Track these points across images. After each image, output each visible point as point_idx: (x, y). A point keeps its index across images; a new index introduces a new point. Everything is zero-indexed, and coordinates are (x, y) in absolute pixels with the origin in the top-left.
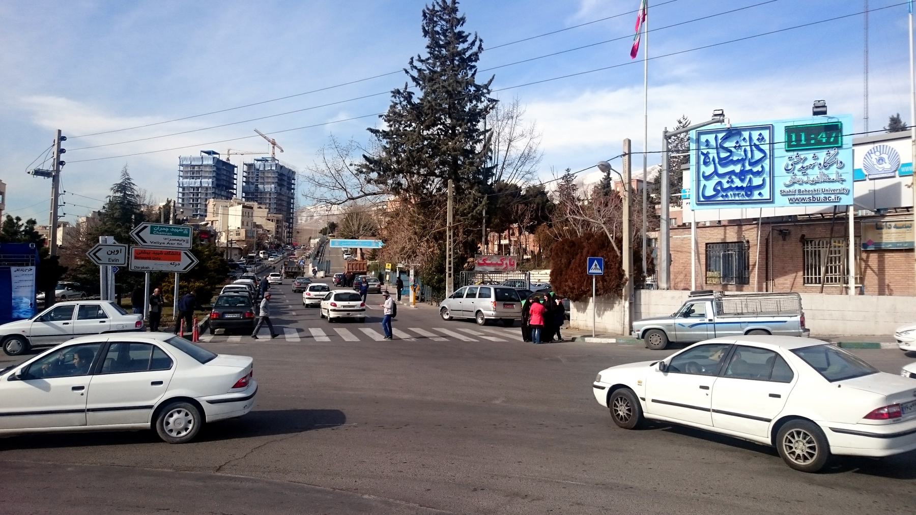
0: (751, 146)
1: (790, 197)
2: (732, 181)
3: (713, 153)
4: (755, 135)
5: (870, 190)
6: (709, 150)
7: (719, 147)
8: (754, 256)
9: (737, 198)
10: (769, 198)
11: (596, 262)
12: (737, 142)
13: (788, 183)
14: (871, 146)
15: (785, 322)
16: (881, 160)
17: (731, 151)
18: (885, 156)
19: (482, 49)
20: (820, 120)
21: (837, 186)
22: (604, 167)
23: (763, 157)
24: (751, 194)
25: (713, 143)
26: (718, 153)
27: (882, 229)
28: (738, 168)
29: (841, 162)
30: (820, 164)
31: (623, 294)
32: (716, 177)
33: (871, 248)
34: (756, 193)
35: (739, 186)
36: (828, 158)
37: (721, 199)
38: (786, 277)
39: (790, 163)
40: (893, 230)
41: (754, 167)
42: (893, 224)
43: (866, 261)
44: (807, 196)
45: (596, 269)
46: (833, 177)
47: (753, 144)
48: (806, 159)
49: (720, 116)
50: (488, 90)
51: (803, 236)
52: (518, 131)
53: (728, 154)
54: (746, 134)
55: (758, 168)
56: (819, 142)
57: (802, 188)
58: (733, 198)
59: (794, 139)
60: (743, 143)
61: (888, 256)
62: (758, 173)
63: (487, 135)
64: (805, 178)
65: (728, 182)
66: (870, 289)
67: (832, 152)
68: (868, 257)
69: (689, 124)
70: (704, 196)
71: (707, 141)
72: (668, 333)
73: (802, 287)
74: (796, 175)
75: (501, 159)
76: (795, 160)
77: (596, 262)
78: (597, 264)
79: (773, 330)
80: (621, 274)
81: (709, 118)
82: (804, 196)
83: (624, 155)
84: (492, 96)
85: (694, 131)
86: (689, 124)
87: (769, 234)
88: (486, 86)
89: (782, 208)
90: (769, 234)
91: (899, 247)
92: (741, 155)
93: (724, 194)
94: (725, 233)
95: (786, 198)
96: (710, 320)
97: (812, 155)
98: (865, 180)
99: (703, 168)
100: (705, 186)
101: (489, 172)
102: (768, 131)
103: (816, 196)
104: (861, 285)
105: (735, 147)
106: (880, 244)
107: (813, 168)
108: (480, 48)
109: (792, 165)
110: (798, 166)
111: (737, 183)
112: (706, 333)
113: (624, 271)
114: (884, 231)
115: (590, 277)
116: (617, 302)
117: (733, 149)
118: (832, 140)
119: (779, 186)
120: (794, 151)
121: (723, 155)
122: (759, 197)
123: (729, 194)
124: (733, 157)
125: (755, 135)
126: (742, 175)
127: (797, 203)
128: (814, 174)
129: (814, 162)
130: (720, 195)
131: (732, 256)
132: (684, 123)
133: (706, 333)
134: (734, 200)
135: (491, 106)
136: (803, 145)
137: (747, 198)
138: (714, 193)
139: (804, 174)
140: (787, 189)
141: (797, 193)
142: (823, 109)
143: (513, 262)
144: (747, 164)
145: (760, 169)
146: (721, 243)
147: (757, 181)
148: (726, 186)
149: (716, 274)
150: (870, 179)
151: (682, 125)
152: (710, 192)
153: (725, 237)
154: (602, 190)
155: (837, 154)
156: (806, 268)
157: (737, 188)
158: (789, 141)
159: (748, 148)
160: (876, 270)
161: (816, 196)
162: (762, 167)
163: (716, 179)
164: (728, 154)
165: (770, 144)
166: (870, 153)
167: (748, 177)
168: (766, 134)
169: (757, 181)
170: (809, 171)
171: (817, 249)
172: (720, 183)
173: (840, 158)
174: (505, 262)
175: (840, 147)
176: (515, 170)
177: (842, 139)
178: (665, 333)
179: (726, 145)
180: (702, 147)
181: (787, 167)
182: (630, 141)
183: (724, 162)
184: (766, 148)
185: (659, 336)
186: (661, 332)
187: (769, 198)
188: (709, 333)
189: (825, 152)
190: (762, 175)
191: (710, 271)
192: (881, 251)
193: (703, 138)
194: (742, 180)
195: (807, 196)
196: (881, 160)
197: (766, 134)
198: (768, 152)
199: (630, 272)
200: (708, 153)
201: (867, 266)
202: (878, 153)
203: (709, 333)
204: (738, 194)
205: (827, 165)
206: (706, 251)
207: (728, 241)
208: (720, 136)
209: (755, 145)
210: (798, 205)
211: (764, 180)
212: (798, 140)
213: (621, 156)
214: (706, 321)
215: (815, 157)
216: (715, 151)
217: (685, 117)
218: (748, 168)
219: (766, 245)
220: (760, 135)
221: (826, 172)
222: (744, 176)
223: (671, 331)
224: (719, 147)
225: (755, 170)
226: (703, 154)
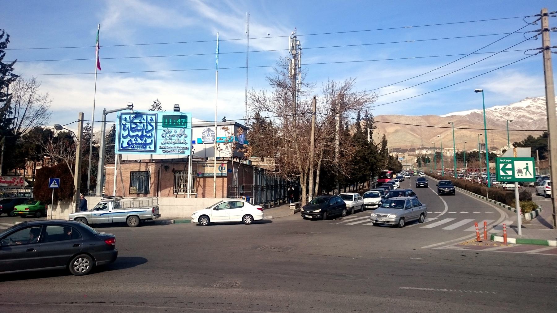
0: (146, 123)
1: (163, 150)
2: (137, 140)
3: (128, 125)
4: (149, 117)
5: (204, 149)
6: (126, 123)
7: (131, 122)
8: (152, 179)
9: (139, 149)
10: (153, 150)
11: (55, 181)
12: (140, 120)
13: (163, 143)
14: (205, 128)
15: (146, 211)
16: (208, 135)
17: (137, 125)
18: (210, 133)
19: (9, 41)
20: (177, 114)
21: (184, 146)
22: (57, 127)
23: (152, 129)
24: (146, 147)
25: (128, 119)
26: (130, 125)
27: (205, 167)
28: (140, 134)
29: (186, 135)
30: (177, 135)
31: (73, 199)
32: (129, 137)
33: (200, 176)
34: (148, 147)
35: (140, 142)
36: (181, 132)
37: (131, 149)
38: (166, 190)
39: (164, 133)
40: (209, 168)
41: (148, 133)
42: (209, 165)
43: (199, 182)
44: (171, 150)
45: (55, 184)
46: (182, 141)
47: (147, 122)
48: (171, 132)
49: (131, 106)
50: (12, 68)
51: (174, 169)
52: (35, 97)
53: (136, 126)
54: (145, 117)
55: (149, 134)
56: (177, 124)
57: (169, 146)
58: (137, 149)
59: (170, 122)
60: (143, 121)
61: (207, 179)
62: (149, 137)
63: (9, 97)
64: (170, 141)
65: (135, 140)
66: (200, 195)
67: (183, 129)
68: (199, 180)
69: (160, 104)
70: (122, 147)
71: (125, 118)
72: (88, 219)
73: (172, 194)
74: (166, 139)
75: (21, 113)
76: (167, 132)
77: (55, 181)
78: (55, 182)
79: (140, 215)
80: (73, 187)
81: (126, 107)
82: (169, 150)
83: (79, 121)
84: (14, 72)
85: (119, 112)
86: (160, 104)
87: (160, 168)
88: (10, 66)
89: (160, 155)
90: (160, 168)
91: (211, 175)
92: (142, 127)
93: (133, 146)
94: (140, 166)
95: (162, 150)
96: (110, 212)
97: (174, 130)
98: (202, 144)
99: (123, 132)
100: (123, 141)
101: (9, 121)
102: (155, 116)
103: (175, 150)
104: (196, 194)
105: (139, 123)
106: (204, 174)
107: (174, 136)
108: (7, 40)
109: (165, 134)
110: (168, 135)
111: (139, 141)
112: (107, 218)
113: (74, 186)
114: (206, 168)
115: (51, 189)
116: (71, 204)
117: (138, 124)
118: (183, 124)
119: (159, 144)
120: (166, 127)
121: (133, 126)
122: (149, 149)
123: (135, 146)
124: (138, 127)
125: (149, 117)
126: (141, 137)
127: (166, 153)
128: (174, 139)
129: (175, 133)
130: (130, 146)
131: (143, 179)
132: (157, 103)
133: (107, 218)
134: (137, 150)
135: (12, 79)
136: (170, 125)
137: (144, 149)
138: (128, 145)
139: (170, 139)
140: (162, 146)
141: (166, 148)
142: (178, 109)
143: (23, 181)
144: (144, 132)
145: (150, 135)
146: (138, 172)
147: (149, 141)
148: (134, 142)
149: (135, 188)
150: (204, 143)
151: (156, 104)
152: (125, 145)
153: (140, 168)
154: (110, 138)
155: (185, 130)
156: (175, 186)
157: (139, 144)
158: (164, 123)
159: (145, 124)
160: (202, 186)
161: (175, 150)
162: (151, 134)
163: (129, 138)
164: (136, 126)
165: (155, 123)
166: (204, 131)
167: (145, 138)
168: (154, 117)
169: (149, 141)
170: (172, 138)
171: (180, 176)
172: (130, 140)
173: (186, 132)
174: (16, 181)
175: (186, 127)
176: (31, 122)
177: (187, 124)
178: (86, 219)
179: (135, 121)
180: (123, 121)
181: (163, 135)
182: (83, 114)
183: (133, 130)
184: (153, 124)
185: (83, 221)
186: (85, 219)
187: (153, 150)
188: (109, 218)
189: (180, 129)
190: (151, 138)
191: (132, 186)
192: (204, 177)
193: (124, 116)
194: (142, 140)
195: (171, 150)
196: (208, 135)
197: (154, 117)
198: (154, 126)
199: (78, 186)
200: (126, 124)
201: (199, 184)
202: (207, 132)
203: (109, 218)
204: (139, 147)
205: (180, 136)
206: (131, 176)
207: (141, 171)
208: (132, 116)
209: (149, 123)
210: (167, 154)
211: (152, 140)
212: (168, 122)
213: (77, 121)
214: (108, 212)
215: (175, 131)
216: (129, 124)
217: (158, 100)
218: (145, 134)
219: (158, 174)
220: (151, 118)
221: (179, 139)
222: (143, 138)
223: (89, 218)
224: (131, 122)
225: (148, 135)
226: (123, 124)
